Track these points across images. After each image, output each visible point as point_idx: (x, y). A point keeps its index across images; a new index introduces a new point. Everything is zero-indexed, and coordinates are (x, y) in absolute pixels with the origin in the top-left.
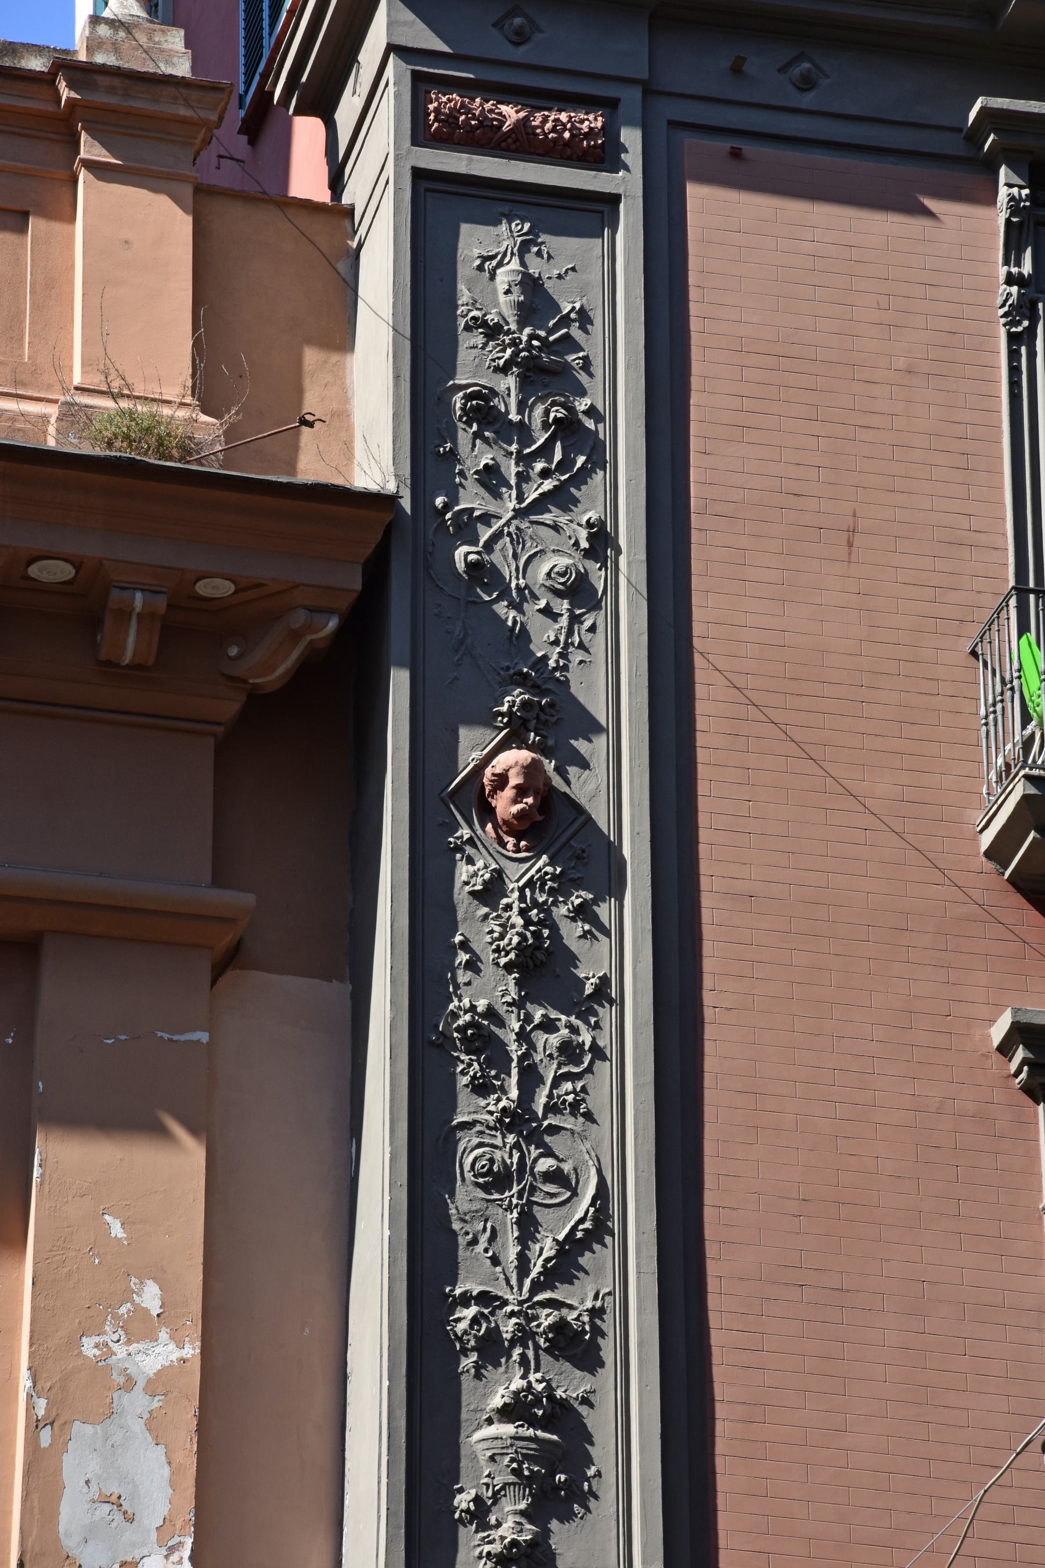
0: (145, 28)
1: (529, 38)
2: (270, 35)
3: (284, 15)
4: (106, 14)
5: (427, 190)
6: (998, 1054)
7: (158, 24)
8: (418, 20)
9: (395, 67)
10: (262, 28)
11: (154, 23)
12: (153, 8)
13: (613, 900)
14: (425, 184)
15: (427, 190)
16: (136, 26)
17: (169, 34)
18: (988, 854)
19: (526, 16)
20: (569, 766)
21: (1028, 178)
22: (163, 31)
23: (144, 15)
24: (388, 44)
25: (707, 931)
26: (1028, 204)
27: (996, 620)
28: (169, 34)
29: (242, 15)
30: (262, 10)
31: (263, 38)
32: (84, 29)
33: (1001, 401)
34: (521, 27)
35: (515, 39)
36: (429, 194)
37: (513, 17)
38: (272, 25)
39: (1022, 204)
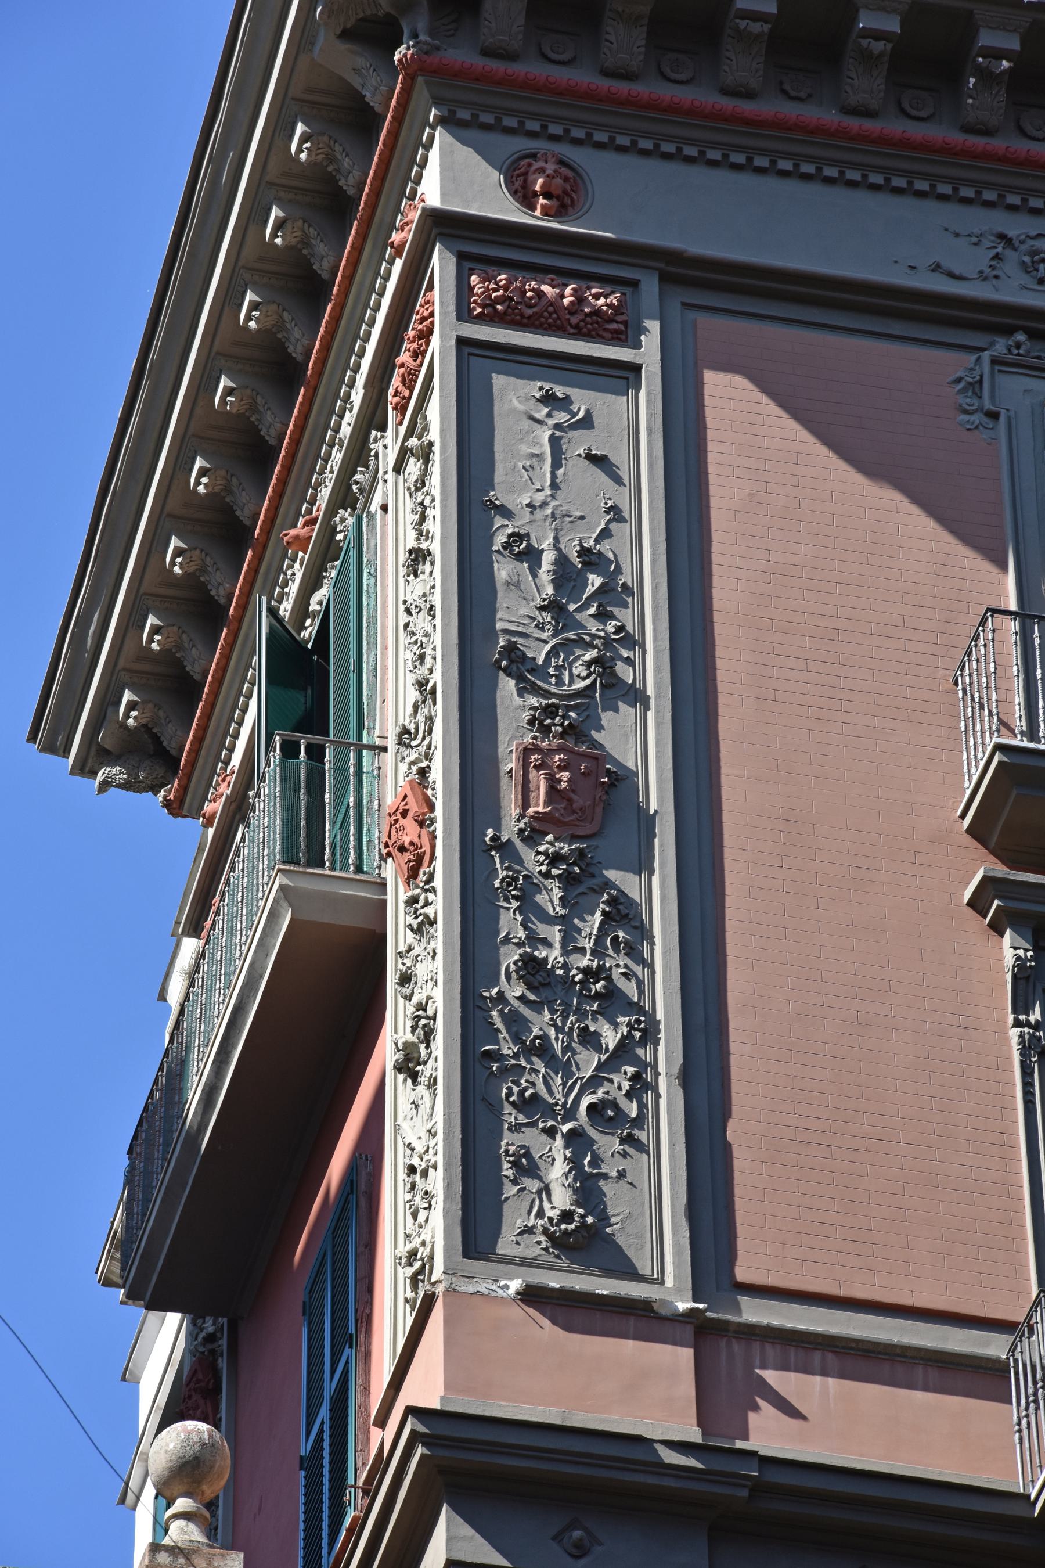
0: (205, 1554)
1: (589, 1550)
2: (329, 1553)
3: (343, 1534)
4: (166, 1541)
5: (470, 354)
6: (970, 911)
7: (218, 1548)
8: (477, 1535)
9: (441, 259)
10: (321, 1548)
11: (214, 1547)
12: (213, 1531)
13: (649, 1092)
14: (467, 350)
15: (470, 354)
16: (195, 1551)
17: (228, 1557)
18: (970, 904)
19: (585, 1529)
20: (607, 869)
21: (1031, 939)
22: (223, 1555)
23: (204, 1540)
24: (447, 1560)
25: (740, 1230)
26: (1033, 964)
27: (1019, 1343)
28: (228, 1557)
29: (301, 1535)
30: (321, 1529)
31: (322, 1521)
32: (143, 1558)
33: (1028, 1256)
34: (581, 1539)
35: (574, 1551)
36: (471, 358)
37: (572, 1530)
38: (332, 1544)
39: (1028, 964)
